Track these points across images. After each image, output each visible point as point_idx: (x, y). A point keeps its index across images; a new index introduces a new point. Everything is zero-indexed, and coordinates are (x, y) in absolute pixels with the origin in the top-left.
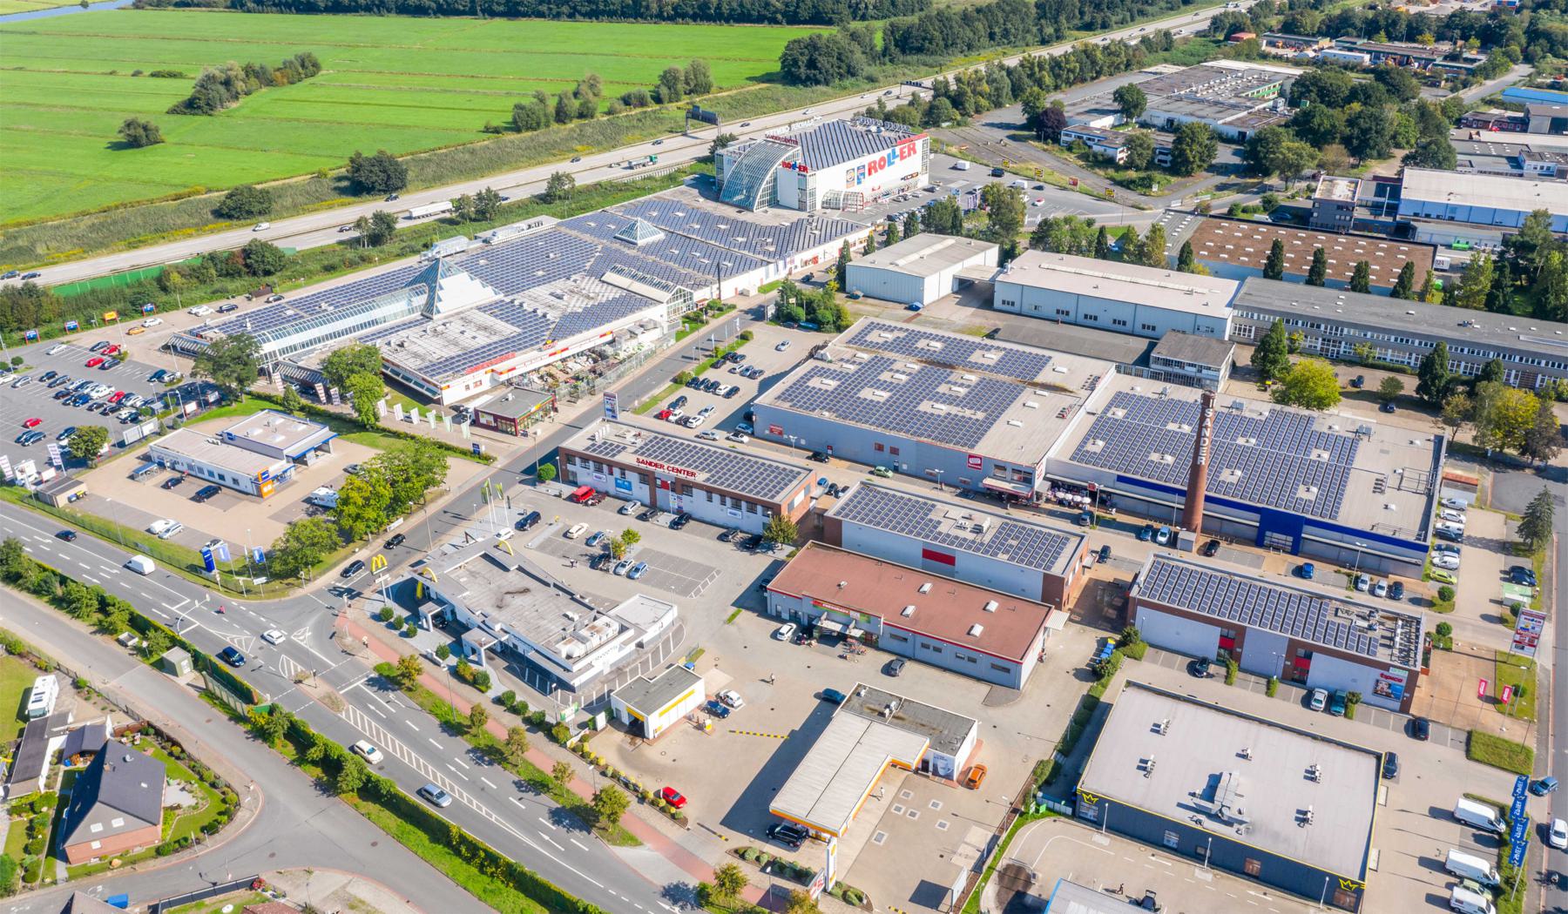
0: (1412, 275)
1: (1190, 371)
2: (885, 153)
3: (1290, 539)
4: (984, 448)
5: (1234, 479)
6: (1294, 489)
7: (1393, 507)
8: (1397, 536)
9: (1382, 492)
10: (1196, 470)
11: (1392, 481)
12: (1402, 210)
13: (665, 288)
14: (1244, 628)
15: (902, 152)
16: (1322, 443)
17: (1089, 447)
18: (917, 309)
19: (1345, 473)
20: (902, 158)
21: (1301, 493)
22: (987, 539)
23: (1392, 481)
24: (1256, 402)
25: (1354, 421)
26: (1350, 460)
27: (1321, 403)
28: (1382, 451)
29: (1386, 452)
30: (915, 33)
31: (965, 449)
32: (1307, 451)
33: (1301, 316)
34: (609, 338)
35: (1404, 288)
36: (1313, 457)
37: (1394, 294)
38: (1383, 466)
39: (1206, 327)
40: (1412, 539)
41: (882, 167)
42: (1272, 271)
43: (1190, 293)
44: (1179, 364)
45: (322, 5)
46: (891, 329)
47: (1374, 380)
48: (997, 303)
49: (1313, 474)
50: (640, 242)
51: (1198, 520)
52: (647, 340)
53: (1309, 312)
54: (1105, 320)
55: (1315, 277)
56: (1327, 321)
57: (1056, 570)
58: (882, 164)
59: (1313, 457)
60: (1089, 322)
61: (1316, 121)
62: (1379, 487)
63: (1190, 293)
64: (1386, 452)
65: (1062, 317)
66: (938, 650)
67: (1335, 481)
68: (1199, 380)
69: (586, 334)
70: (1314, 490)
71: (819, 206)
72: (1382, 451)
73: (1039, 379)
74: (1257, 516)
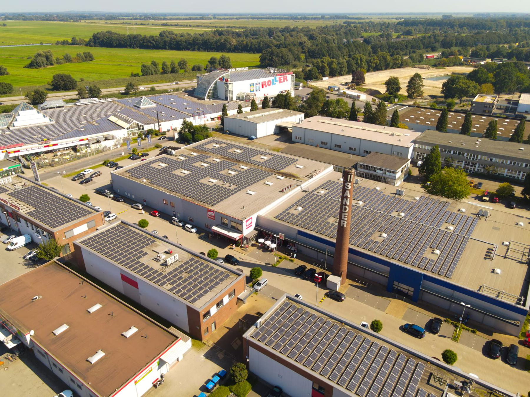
0: (523, 129)
1: (379, 173)
2: (271, 79)
3: (412, 289)
4: (221, 208)
5: (380, 240)
6: (423, 249)
7: (498, 271)
8: (499, 299)
9: (491, 259)
10: (341, 230)
11: (500, 250)
12: (518, 110)
13: (128, 122)
14: (332, 388)
15: (280, 80)
16: (451, 220)
17: (292, 211)
18: (252, 139)
19: (464, 240)
20: (280, 82)
21: (427, 254)
22: (168, 270)
23: (500, 250)
24: (416, 192)
25: (476, 207)
26: (469, 232)
27: (457, 196)
28: (494, 228)
29: (498, 229)
30: (317, 52)
31: (206, 206)
32: (439, 224)
33: (452, 148)
34: (86, 142)
35: (518, 136)
36: (443, 228)
37: (512, 139)
38: (494, 239)
39: (399, 153)
40: (512, 302)
41: (269, 85)
42: (441, 126)
43: (392, 135)
44: (375, 169)
45: (115, 44)
46: (265, 154)
47: (493, 186)
48: (294, 139)
49: (440, 240)
50: (141, 107)
51: (344, 267)
52: (109, 144)
53: (458, 146)
54: (346, 147)
55: (465, 129)
56: (468, 151)
57: (199, 306)
58: (269, 83)
59: (443, 228)
60: (337, 148)
61: (479, 75)
62: (488, 255)
63: (392, 135)
64: (498, 229)
65: (324, 145)
66: (61, 371)
67: (455, 247)
68: (385, 179)
69: (73, 139)
70: (438, 252)
71: (235, 99)
72: (494, 228)
73: (286, 170)
74: (388, 268)
